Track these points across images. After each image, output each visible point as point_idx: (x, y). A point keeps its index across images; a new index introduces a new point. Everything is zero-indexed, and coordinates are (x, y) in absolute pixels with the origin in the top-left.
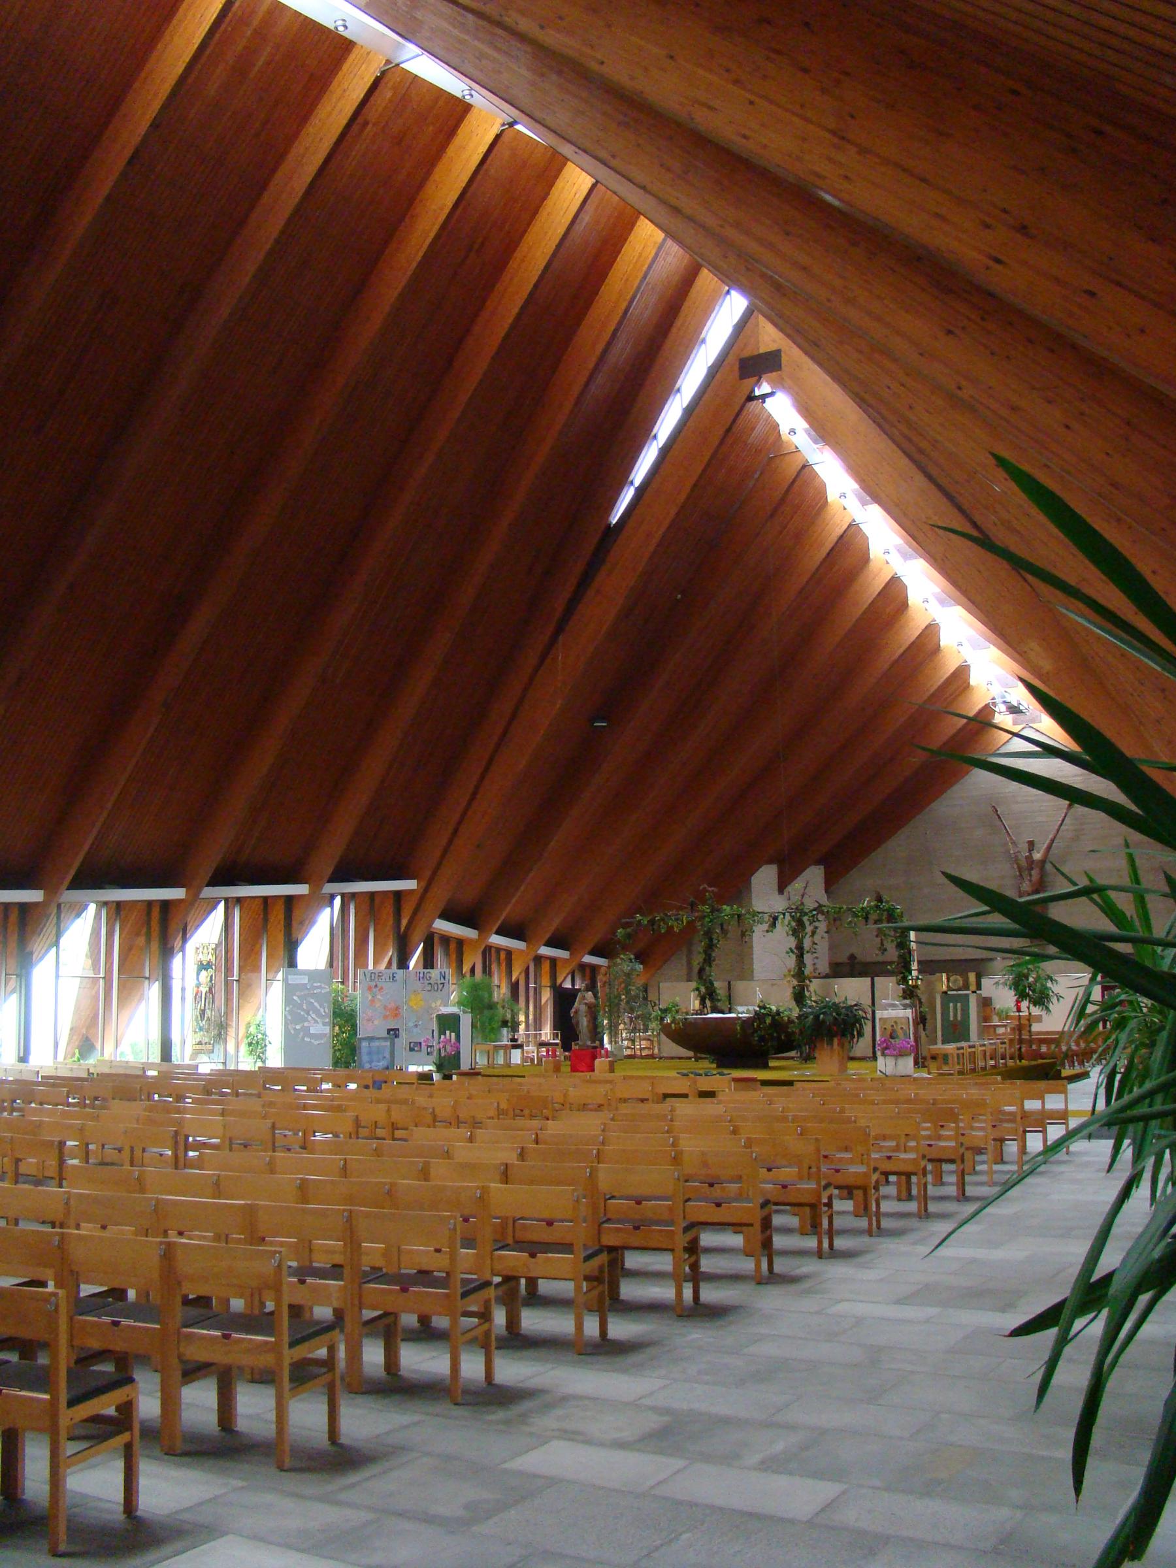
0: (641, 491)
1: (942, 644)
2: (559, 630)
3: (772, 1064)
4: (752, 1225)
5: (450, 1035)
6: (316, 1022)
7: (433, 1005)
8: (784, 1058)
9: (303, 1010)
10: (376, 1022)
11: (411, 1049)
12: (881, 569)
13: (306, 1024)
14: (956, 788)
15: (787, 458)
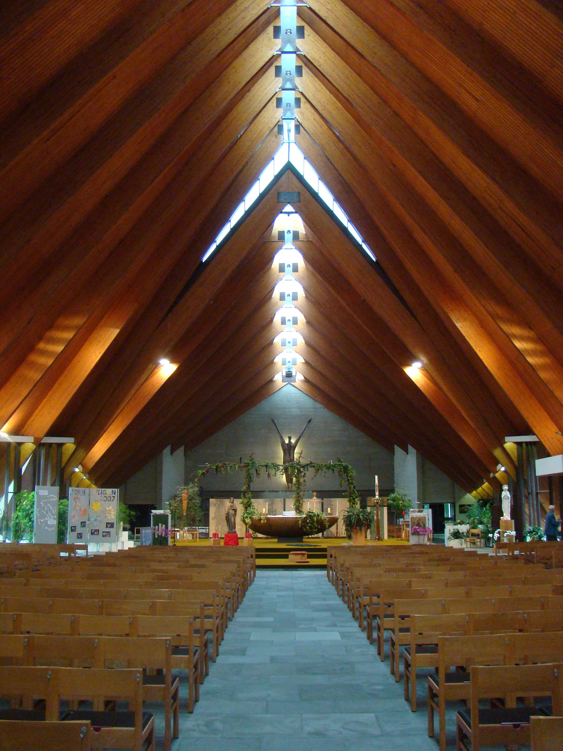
0: (219, 248)
1: (275, 341)
2: (170, 311)
3: (304, 540)
4: (212, 630)
5: (161, 527)
6: (50, 518)
7: (107, 509)
8: (314, 538)
9: (45, 510)
10: (76, 518)
11: (92, 534)
12: (277, 303)
13: (46, 519)
14: (253, 408)
15: (274, 244)
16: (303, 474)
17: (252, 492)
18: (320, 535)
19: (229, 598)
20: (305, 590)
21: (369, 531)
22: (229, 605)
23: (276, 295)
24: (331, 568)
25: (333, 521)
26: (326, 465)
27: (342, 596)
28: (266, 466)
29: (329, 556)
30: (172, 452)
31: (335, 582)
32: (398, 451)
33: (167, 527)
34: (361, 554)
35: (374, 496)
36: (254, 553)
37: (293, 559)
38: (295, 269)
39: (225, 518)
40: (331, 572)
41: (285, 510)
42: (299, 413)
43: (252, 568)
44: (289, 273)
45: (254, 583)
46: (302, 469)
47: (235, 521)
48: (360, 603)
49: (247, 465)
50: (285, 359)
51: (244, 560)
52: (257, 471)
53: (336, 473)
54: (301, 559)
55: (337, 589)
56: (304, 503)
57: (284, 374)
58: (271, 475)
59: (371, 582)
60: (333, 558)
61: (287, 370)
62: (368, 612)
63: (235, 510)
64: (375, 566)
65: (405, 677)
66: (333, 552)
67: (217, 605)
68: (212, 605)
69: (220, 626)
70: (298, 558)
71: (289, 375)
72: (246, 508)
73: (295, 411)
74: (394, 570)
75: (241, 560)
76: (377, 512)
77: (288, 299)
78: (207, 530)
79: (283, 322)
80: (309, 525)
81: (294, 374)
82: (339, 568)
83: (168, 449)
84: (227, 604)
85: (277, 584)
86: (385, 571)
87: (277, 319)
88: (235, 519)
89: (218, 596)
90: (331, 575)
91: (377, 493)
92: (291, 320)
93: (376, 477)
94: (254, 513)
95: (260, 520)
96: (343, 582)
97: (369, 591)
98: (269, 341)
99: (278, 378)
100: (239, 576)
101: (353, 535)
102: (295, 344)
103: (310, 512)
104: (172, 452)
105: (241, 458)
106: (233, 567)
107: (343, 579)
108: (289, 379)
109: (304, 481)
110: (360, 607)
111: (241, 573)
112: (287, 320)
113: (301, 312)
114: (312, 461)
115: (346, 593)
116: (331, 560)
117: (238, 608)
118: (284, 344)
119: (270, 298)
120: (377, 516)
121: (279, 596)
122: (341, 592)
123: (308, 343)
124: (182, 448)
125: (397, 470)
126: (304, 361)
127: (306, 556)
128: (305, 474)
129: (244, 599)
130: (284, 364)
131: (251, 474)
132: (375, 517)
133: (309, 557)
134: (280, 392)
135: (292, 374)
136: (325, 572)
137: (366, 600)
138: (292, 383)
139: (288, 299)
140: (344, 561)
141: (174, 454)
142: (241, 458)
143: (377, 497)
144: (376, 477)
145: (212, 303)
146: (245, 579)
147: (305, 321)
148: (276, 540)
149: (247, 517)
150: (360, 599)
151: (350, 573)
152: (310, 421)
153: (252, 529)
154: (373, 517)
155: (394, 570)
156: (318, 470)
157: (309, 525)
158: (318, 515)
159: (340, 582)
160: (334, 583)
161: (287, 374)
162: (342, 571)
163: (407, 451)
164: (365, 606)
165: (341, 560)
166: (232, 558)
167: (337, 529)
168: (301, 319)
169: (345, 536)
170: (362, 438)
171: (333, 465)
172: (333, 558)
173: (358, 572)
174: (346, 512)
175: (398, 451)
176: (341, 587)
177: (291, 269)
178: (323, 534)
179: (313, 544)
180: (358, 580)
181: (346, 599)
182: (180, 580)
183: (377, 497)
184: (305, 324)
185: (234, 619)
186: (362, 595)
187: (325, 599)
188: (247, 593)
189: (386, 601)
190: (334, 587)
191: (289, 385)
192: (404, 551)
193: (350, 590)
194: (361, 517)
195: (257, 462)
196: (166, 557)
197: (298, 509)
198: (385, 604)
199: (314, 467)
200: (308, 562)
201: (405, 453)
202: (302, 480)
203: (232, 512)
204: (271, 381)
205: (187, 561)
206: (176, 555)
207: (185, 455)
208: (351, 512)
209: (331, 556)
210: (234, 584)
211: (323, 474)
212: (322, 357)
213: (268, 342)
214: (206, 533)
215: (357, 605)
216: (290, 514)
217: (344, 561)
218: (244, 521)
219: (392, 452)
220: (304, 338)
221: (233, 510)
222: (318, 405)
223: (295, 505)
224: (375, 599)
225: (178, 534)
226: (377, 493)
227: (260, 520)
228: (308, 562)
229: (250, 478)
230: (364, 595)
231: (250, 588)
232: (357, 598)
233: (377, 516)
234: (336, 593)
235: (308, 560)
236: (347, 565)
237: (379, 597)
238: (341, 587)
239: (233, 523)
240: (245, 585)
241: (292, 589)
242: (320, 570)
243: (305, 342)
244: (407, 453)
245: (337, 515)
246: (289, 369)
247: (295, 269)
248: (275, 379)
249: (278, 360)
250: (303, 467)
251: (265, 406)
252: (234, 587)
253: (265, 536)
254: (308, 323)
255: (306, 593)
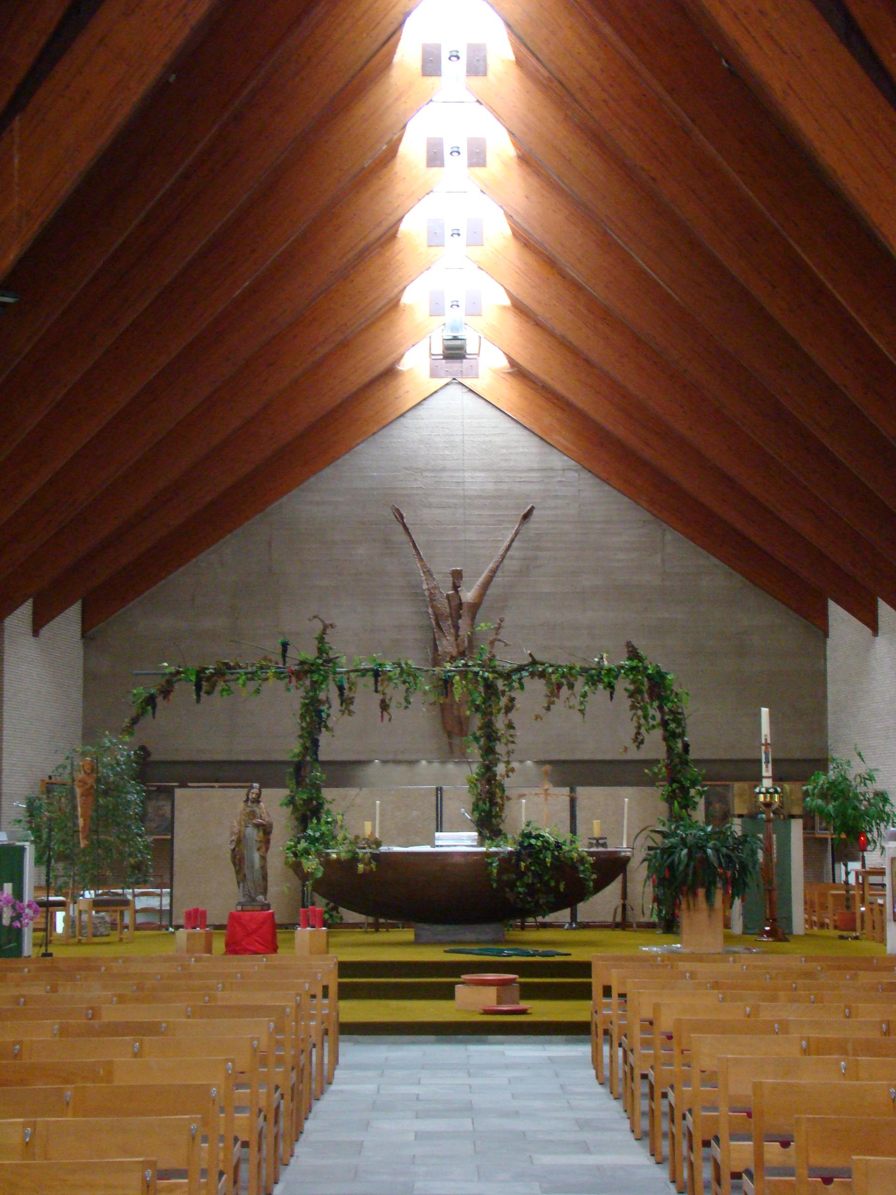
1: (404, 227)
14: (328, 471)
16: (503, 701)
17: (323, 763)
18: (563, 915)
19: (245, 1144)
20: (516, 1114)
21: (737, 902)
22: (244, 1167)
23: (407, 54)
24: (606, 1032)
25: (611, 867)
26: (584, 670)
27: (648, 1137)
28: (376, 674)
29: (597, 991)
30: (38, 624)
31: (623, 1084)
32: (841, 620)
33: (18, 893)
34: (716, 985)
35: (759, 779)
36: (333, 982)
37: (472, 999)
38: (477, 67)
39: (229, 855)
40: (606, 1049)
41: (439, 828)
42: (490, 487)
43: (326, 1032)
44: (455, 248)
45: (333, 1087)
46: (500, 684)
47: (264, 868)
48: (717, 1167)
49: (305, 670)
50: (438, 47)
51: (298, 1006)
52: (341, 688)
53: (623, 700)
54: (499, 1002)
55: (630, 1111)
56: (507, 803)
57: (439, 349)
58: (393, 705)
59: (757, 1087)
60: (614, 1000)
61: (449, 334)
62: (671, 1105)
63: (266, 830)
64: (768, 1029)
65: (670, 1136)
66: (614, 978)
67: (204, 1173)
68: (182, 1174)
69: (294, 1112)
70: (488, 997)
71: (454, 352)
72: (303, 821)
73: (476, 482)
74: (840, 1047)
75: (290, 1006)
76: (769, 838)
77: (456, 165)
78: (166, 901)
79: (435, 159)
80: (528, 879)
81: (470, 348)
82: (637, 1034)
83: (25, 611)
84: (236, 1168)
85: (414, 1090)
86: (806, 1051)
87: (411, 150)
88: (263, 858)
89: (205, 1139)
90: (606, 1060)
91: (767, 771)
92: (463, 55)
93: (765, 711)
94: (334, 838)
95: (354, 859)
96: (651, 1087)
97: (749, 1119)
98: (385, 225)
99: (416, 364)
100: (280, 1061)
101: (684, 919)
102: (475, 240)
103: (528, 836)
104: (38, 624)
105: (285, 646)
106: (259, 1031)
107: (651, 1073)
108: (455, 365)
109: (510, 726)
110: (718, 1181)
111: (288, 1053)
112: (447, 151)
113: (499, 118)
114: (538, 657)
115: (665, 1125)
116: (608, 1006)
117: (276, 1182)
118: (435, 240)
119: (387, 64)
120: (768, 851)
121: (418, 1135)
122: (645, 1124)
123: (524, 239)
124: (74, 613)
125: (835, 691)
126: (507, 302)
127: (515, 991)
128: (512, 700)
129: (299, 1149)
130: (436, 311)
131: (320, 702)
132: (760, 855)
133: (529, 992)
134: (421, 412)
135: (462, 348)
136: (583, 1050)
137: (739, 1153)
138: (466, 382)
139: (453, 72)
140: (657, 1007)
141: (45, 631)
142: (285, 646)
143: (767, 783)
144: (765, 711)
145: (172, 78)
146: (301, 1071)
147: (513, 58)
148: (408, 935)
149: (307, 852)
150: (716, 1151)
151: (676, 1052)
152: (526, 516)
153: (324, 895)
154: (754, 853)
155: (840, 1047)
156: (559, 686)
157: (528, 879)
158: (558, 846)
159: (642, 1088)
160: (620, 1089)
161: (447, 348)
162: (646, 1044)
163: (872, 624)
164: (736, 1176)
165: (644, 1002)
166: (261, 998)
167: (624, 895)
168: (502, 148)
169: (655, 919)
170: (713, 576)
171: (610, 670)
172: (614, 1000)
173: (709, 1051)
174: (658, 838)
175: (841, 620)
176: (644, 1105)
177: (462, 64)
178: (574, 916)
179: (541, 949)
180: (710, 1078)
181: (665, 1147)
182: (67, 1081)
183: (767, 783)
184: (514, 164)
185: (293, 1161)
186: (724, 1135)
187: (585, 1148)
188: (308, 1125)
189: (817, 1160)
190: (616, 1106)
191: (455, 390)
192: (865, 978)
193: (678, 1115)
194: (709, 851)
195: (343, 660)
196: (16, 1000)
197: (488, 823)
198: (813, 1171)
199: (542, 675)
200: (523, 1012)
201: (868, 631)
202: (500, 723)
203: (252, 834)
204: (390, 373)
205: (95, 1013)
206: (54, 990)
207: (84, 635)
208: (673, 834)
209: (607, 991)
210: (263, 1091)
211: (575, 701)
212: (576, 287)
213: (380, 231)
214: (160, 912)
215: (706, 1172)
216: (459, 841)
217: (657, 1007)
218: (297, 867)
219: (820, 625)
220: (509, 217)
221: (258, 826)
222: (558, 461)
223: (476, 807)
224: (773, 1150)
225: (60, 916)
226: (767, 771)
227: (354, 859)
228: (523, 1012)
229: (319, 712)
230: (734, 1137)
231: (319, 1107)
232: (706, 1144)
233: (768, 851)
234: (627, 1124)
235: (524, 1004)
236: (666, 1023)
237: (785, 1144)
238: (644, 1105)
239: (258, 874)
240: (301, 1093)
241: (468, 1109)
242: (567, 1042)
243: (515, 234)
244: (875, 630)
245: (623, 846)
246: (454, 328)
247: (477, 67)
248: (404, 365)
249: (415, 298)
250: (507, 676)
251: (369, 463)
252: (263, 1103)
253: (371, 920)
254: (526, 159)
255: (520, 1125)
